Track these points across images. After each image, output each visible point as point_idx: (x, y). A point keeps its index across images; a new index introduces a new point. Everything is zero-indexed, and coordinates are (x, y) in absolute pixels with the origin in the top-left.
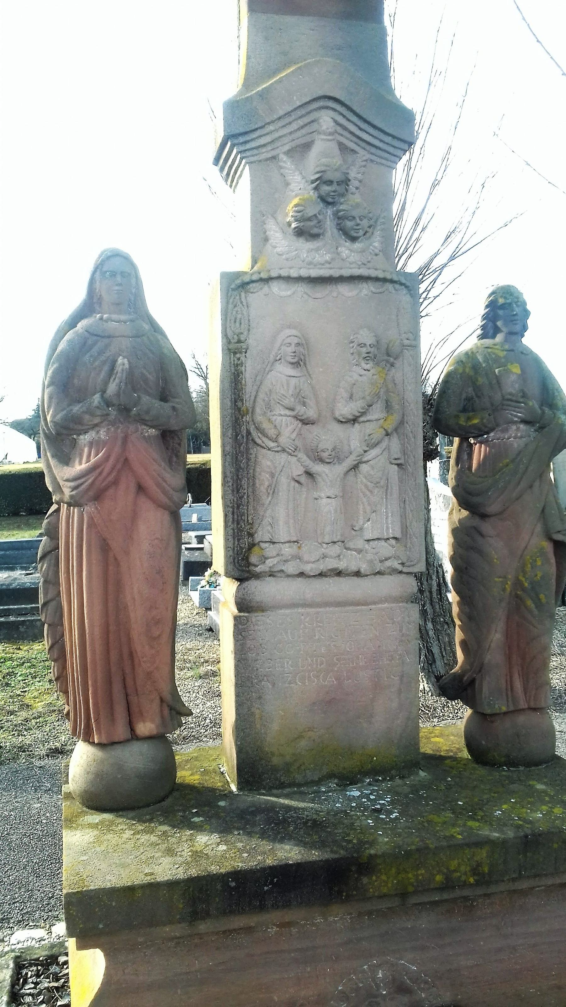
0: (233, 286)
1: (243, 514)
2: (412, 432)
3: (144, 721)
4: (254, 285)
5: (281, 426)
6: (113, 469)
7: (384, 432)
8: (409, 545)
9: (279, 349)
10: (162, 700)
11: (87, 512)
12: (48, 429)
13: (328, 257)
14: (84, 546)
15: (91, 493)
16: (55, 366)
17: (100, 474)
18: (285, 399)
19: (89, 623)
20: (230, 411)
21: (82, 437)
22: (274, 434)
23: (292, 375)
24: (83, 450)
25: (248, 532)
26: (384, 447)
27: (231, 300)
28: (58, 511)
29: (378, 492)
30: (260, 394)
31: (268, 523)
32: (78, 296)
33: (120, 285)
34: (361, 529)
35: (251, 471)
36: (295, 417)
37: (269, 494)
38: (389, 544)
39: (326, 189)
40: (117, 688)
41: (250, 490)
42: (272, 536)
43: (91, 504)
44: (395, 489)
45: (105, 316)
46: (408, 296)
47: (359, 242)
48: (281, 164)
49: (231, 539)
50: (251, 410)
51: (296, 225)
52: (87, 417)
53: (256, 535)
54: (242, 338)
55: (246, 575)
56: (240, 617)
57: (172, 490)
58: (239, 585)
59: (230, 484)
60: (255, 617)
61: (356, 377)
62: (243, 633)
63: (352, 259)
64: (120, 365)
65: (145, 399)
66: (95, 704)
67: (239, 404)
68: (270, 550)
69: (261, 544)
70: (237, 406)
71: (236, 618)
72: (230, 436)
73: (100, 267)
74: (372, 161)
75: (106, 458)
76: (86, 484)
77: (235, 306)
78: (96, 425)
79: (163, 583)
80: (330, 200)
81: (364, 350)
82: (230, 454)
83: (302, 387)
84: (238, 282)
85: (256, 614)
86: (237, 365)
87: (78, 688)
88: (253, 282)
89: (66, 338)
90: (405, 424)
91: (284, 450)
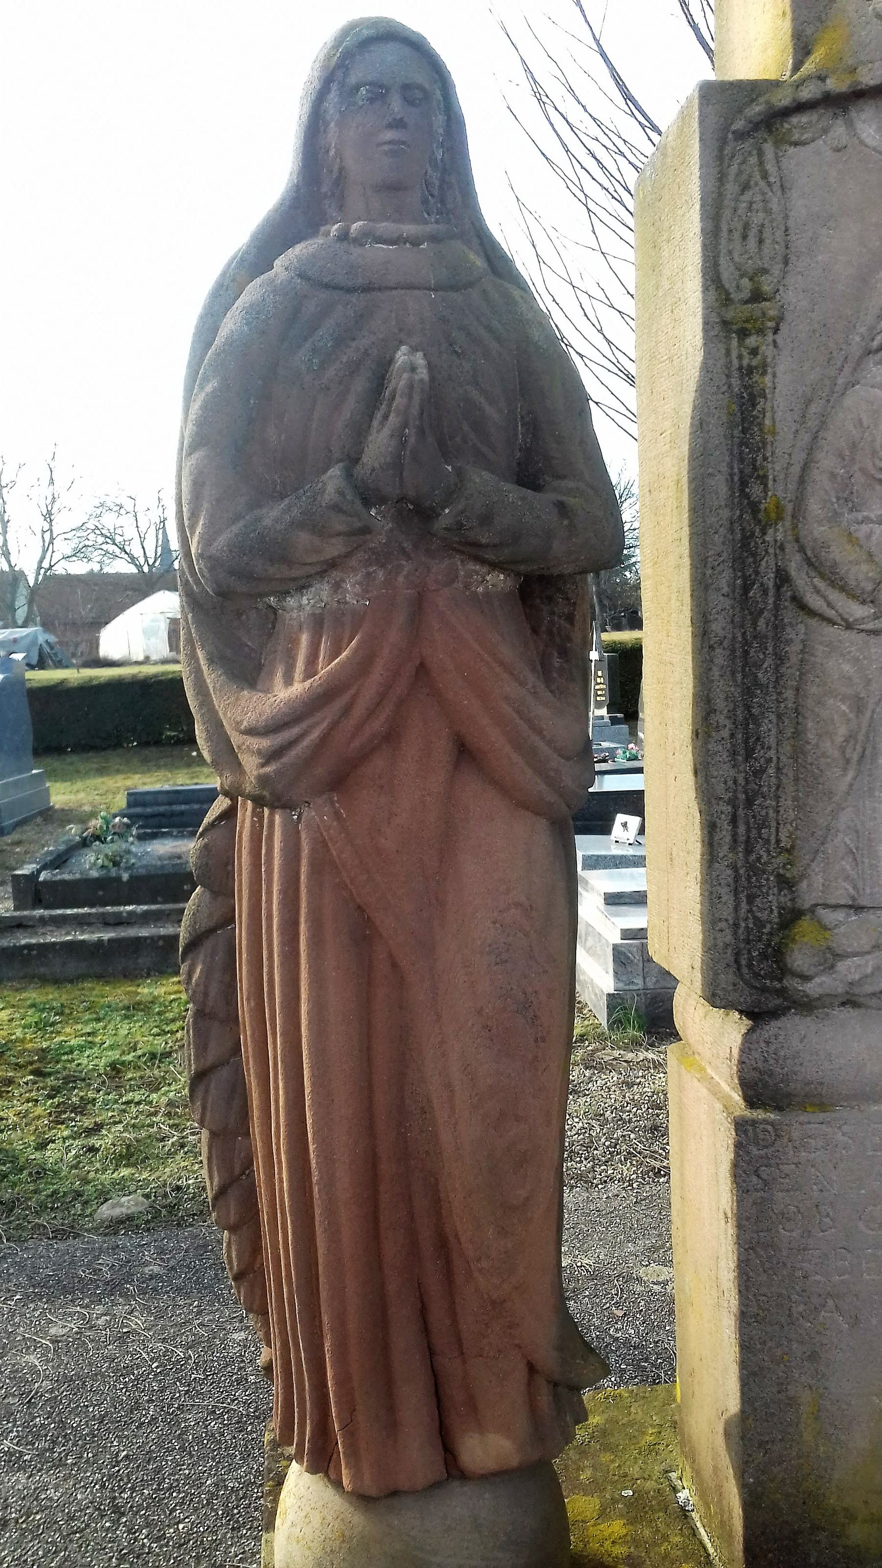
0: (739, 125)
1: (764, 824)
3: (482, 1429)
4: (803, 119)
6: (382, 696)
10: (532, 1369)
11: (308, 826)
12: (198, 582)
14: (303, 927)
15: (320, 771)
16: (209, 388)
17: (346, 711)
19: (320, 1152)
20: (726, 513)
21: (291, 602)
22: (868, 579)
24: (295, 642)
25: (779, 876)
27: (734, 169)
28: (229, 814)
30: (820, 455)
32: (268, 173)
33: (398, 124)
35: (789, 694)
37: (848, 761)
40: (404, 1338)
41: (787, 748)
42: (855, 887)
43: (320, 801)
45: (355, 226)
49: (728, 898)
52: (304, 538)
53: (804, 885)
55: (775, 1002)
56: (754, 1123)
57: (555, 756)
58: (751, 1031)
59: (725, 733)
60: (800, 1124)
62: (764, 1171)
64: (403, 370)
65: (480, 479)
66: (343, 1381)
67: (755, 490)
68: (849, 931)
69: (821, 911)
71: (741, 1126)
72: (726, 590)
73: (339, 74)
75: (362, 665)
76: (306, 742)
77: (745, 187)
78: (332, 565)
79: (536, 1041)
82: (726, 643)
84: (757, 109)
85: (803, 1118)
86: (750, 370)
87: (294, 1328)
88: (800, 107)
89: (239, 302)
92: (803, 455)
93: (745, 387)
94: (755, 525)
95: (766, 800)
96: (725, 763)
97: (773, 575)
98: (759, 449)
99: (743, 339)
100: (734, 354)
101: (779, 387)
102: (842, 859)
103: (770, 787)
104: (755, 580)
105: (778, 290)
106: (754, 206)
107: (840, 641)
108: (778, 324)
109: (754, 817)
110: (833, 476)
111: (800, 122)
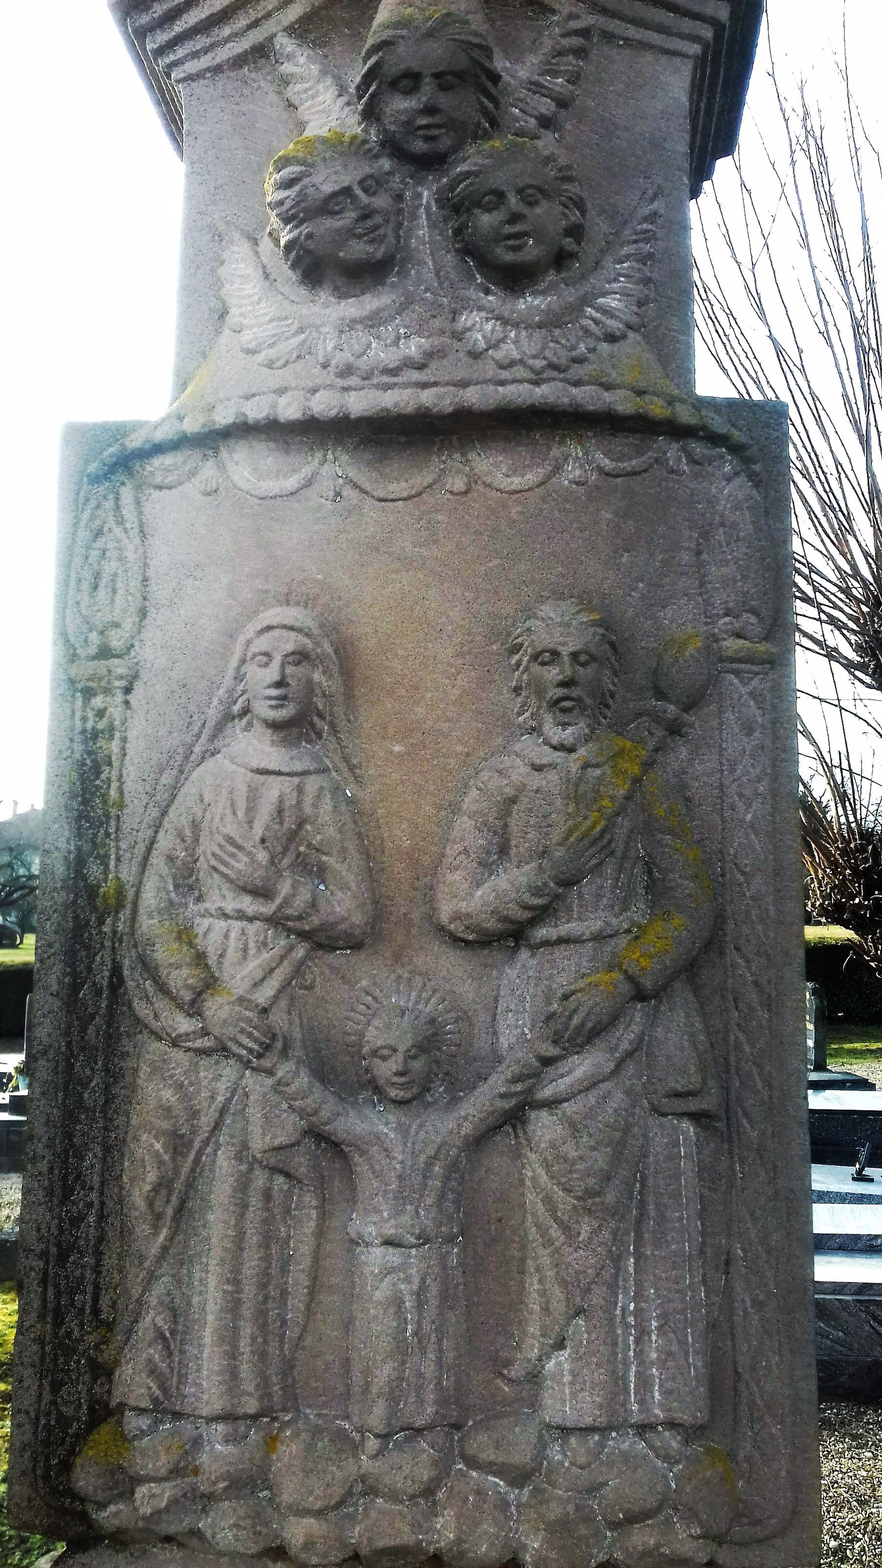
0: (92, 468)
2: (756, 984)
5: (222, 956)
7: (626, 988)
8: (746, 1448)
9: (239, 677)
13: (413, 348)
18: (233, 855)
22: (187, 987)
23: (271, 767)
25: (92, 1361)
26: (625, 1045)
27: (86, 516)
29: (595, 1232)
31: (151, 1334)
34: (535, 1377)
36: (275, 921)
37: (159, 1217)
38: (652, 1447)
39: (400, 105)
42: (162, 1386)
44: (683, 1221)
46: (742, 479)
47: (534, 294)
48: (287, 68)
50: (131, 893)
51: (291, 236)
54: (116, 641)
59: (43, 1166)
61: (520, 771)
63: (508, 351)
70: (84, 878)
74: (608, 37)
77: (98, 533)
80: (419, 146)
81: (553, 674)
82: (51, 1054)
83: (308, 810)
86: (96, 735)
90: (732, 955)
91: (222, 1049)
92: (150, 832)
93: (89, 753)
94: (91, 912)
95: (83, 1257)
96: (40, 1205)
97: (107, 974)
98: (102, 824)
99: (89, 700)
100: (78, 714)
101: (130, 752)
102: (149, 1346)
103: (87, 1240)
104: (86, 978)
105: (132, 646)
106: (108, 554)
107: (164, 1061)
108: (131, 683)
109: (67, 1277)
110: (170, 859)
111: (162, 464)
